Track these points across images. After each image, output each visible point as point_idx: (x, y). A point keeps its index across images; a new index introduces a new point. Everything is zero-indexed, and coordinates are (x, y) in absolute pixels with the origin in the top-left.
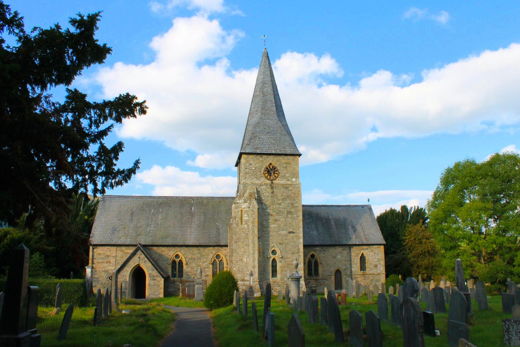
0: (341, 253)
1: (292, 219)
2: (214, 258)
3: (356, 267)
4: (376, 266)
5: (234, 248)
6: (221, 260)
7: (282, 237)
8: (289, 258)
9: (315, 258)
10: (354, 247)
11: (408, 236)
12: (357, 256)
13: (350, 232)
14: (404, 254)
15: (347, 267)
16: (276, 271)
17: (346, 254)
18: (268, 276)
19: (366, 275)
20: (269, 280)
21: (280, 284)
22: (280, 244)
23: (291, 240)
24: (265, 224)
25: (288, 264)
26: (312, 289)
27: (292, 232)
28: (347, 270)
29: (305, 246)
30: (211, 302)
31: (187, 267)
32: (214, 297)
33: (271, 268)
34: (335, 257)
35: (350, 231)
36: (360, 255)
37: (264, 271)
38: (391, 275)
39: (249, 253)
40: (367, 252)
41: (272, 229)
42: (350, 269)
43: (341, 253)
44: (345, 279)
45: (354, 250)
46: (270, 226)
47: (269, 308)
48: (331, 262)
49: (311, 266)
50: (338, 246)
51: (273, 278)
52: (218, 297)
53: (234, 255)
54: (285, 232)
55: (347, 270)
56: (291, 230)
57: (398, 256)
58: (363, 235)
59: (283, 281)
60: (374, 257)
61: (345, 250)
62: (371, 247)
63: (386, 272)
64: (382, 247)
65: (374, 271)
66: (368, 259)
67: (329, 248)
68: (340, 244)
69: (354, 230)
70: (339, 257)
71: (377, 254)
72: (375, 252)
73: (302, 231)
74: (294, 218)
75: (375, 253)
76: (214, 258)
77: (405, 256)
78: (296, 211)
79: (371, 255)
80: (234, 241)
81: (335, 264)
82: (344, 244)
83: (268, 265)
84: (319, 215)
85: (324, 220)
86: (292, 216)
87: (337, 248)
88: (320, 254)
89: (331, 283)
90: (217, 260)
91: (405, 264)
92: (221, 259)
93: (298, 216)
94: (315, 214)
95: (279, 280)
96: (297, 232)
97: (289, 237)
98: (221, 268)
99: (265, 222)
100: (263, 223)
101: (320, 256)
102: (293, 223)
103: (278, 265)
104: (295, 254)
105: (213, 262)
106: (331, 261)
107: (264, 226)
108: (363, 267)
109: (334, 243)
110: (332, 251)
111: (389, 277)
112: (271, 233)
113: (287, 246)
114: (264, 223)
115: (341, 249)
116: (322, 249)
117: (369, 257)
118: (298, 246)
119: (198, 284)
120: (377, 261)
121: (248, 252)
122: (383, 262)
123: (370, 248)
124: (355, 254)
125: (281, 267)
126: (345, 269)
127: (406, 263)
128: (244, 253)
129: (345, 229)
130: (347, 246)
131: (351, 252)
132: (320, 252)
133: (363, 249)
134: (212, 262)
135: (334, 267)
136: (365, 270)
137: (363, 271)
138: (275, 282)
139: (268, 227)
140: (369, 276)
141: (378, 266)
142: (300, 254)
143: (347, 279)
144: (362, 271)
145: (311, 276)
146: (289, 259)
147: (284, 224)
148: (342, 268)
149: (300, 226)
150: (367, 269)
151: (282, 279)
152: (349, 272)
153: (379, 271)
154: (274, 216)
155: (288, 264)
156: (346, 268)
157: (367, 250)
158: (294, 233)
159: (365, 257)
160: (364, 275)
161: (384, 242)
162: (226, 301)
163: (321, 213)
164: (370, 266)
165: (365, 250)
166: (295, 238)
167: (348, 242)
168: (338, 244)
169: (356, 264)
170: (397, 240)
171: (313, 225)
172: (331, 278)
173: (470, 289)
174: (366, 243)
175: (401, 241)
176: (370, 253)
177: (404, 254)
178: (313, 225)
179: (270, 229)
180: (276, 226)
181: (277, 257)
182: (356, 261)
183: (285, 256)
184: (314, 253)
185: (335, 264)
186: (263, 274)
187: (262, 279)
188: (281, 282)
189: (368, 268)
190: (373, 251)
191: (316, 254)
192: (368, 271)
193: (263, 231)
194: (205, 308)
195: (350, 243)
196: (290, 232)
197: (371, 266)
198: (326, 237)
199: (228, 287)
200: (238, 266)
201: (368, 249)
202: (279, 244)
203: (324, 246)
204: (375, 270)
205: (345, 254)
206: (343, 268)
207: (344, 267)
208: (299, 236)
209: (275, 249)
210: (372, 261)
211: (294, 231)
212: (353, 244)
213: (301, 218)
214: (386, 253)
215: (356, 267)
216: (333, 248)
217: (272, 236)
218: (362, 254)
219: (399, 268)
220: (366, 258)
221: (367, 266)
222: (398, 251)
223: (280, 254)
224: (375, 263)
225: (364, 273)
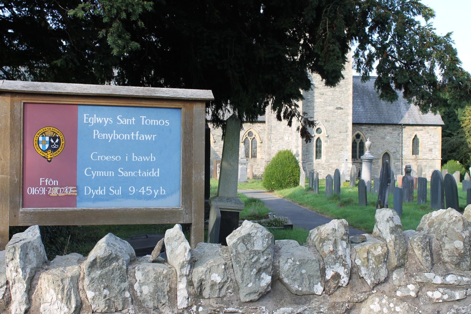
0: (391, 133)
1: (341, 92)
2: (246, 136)
3: (407, 151)
4: (431, 150)
5: (273, 124)
6: (254, 138)
7: (328, 114)
8: (335, 138)
9: (361, 138)
10: (407, 127)
11: (468, 117)
12: (410, 138)
13: (402, 110)
14: (462, 137)
15: (396, 150)
16: (320, 152)
17: (397, 135)
18: (312, 157)
19: (419, 160)
20: (313, 161)
21: (324, 166)
22: (326, 121)
23: (338, 117)
24: (309, 98)
25: (334, 145)
26: (408, 170)
27: (341, 108)
28: (397, 153)
29: (354, 124)
30: (273, 183)
31: (215, 145)
32: (276, 177)
33: (315, 148)
34: (383, 138)
35: (403, 108)
36: (413, 137)
37: (307, 152)
38: (450, 161)
39: (291, 131)
40: (421, 133)
41: (318, 103)
42: (400, 153)
43: (391, 133)
44: (395, 163)
45: (407, 130)
46: (315, 100)
47: (389, 184)
48: (379, 143)
49: (356, 147)
50: (388, 126)
51: (317, 160)
52: (281, 177)
53: (272, 132)
54: (331, 108)
55: (397, 153)
56: (339, 106)
57: (454, 140)
58: (417, 114)
59: (328, 164)
60: (429, 140)
61: (396, 130)
62: (426, 127)
63: (442, 157)
64: (440, 128)
65: (428, 156)
66: (422, 141)
67: (377, 127)
68: (391, 123)
69: (406, 107)
70: (388, 138)
71: (433, 137)
72: (430, 134)
73: (351, 107)
74: (343, 92)
75: (430, 135)
76: (246, 136)
77: (463, 140)
78: (346, 84)
79: (425, 137)
80: (273, 117)
81: (384, 146)
82: (395, 123)
83: (312, 145)
84: (366, 89)
85: (372, 95)
86: (341, 90)
87: (387, 127)
88: (366, 134)
89: (377, 168)
90: (249, 138)
91: (463, 149)
92: (254, 136)
93: (347, 89)
94: (361, 87)
95: (324, 162)
96: (346, 108)
97: (336, 113)
98: (253, 147)
99: (310, 95)
100: (307, 96)
101: (366, 136)
102: (342, 98)
103: (323, 145)
104: (343, 133)
105: (245, 140)
106: (379, 142)
107: (308, 100)
108: (415, 151)
109: (383, 122)
110: (381, 131)
111: (448, 163)
112: (316, 108)
113: (333, 124)
114: (309, 97)
115: (391, 129)
116: (369, 128)
117: (423, 139)
118: (346, 124)
119: (242, 164)
120: (432, 144)
121: (290, 130)
122: (439, 147)
123: (425, 129)
124: (408, 135)
125: (326, 148)
126: (395, 153)
127: (464, 148)
128: (285, 130)
129: (396, 105)
130: (398, 126)
131: (402, 133)
132: (366, 132)
133: (417, 130)
134: (244, 140)
135: (382, 149)
136: (418, 154)
137: (416, 155)
138: (319, 164)
139: (313, 102)
140: (422, 162)
141: (433, 151)
142: (348, 133)
143: (396, 163)
144: (414, 156)
145: (355, 159)
146: (335, 139)
147: (331, 98)
148: (391, 151)
149: (349, 102)
150: (420, 153)
151: (327, 161)
152: (399, 156)
153: (434, 156)
154: (320, 89)
155: (335, 145)
156: (395, 151)
157: (422, 132)
158: (342, 109)
159: (418, 139)
160: (416, 159)
161: (442, 123)
162: (289, 181)
163: (368, 86)
164: (424, 150)
165: (419, 131)
166: (343, 115)
167: (400, 121)
168: (388, 123)
169: (408, 147)
170: (455, 120)
171: (359, 100)
172: (378, 162)
173: (239, 212)
174: (420, 123)
175: (459, 122)
176: (425, 135)
177: (462, 137)
178: (359, 100)
179: (315, 104)
180: (322, 100)
181: (322, 136)
182: (408, 143)
183: (331, 135)
184: (360, 133)
185: (384, 146)
186: (306, 154)
187: (304, 160)
188: (326, 164)
189: (421, 152)
190: (428, 133)
191: (361, 134)
192: (420, 155)
193: (307, 106)
194: (265, 190)
195: (402, 122)
196: (337, 108)
197: (425, 150)
198: (374, 114)
199: (291, 167)
200: (278, 145)
201: (422, 130)
202: (325, 121)
203: (372, 124)
204: (429, 155)
205: (395, 135)
206: (392, 151)
207: (394, 150)
208: (348, 113)
209: (320, 127)
210: (427, 144)
211: (342, 107)
212: (406, 123)
213: (351, 92)
214: (444, 135)
215: (407, 151)
216: (381, 127)
217: (317, 112)
218: (416, 136)
219: (455, 154)
220: (420, 141)
221: (420, 150)
222: (455, 134)
223: (326, 133)
224: (430, 147)
225: (416, 157)
